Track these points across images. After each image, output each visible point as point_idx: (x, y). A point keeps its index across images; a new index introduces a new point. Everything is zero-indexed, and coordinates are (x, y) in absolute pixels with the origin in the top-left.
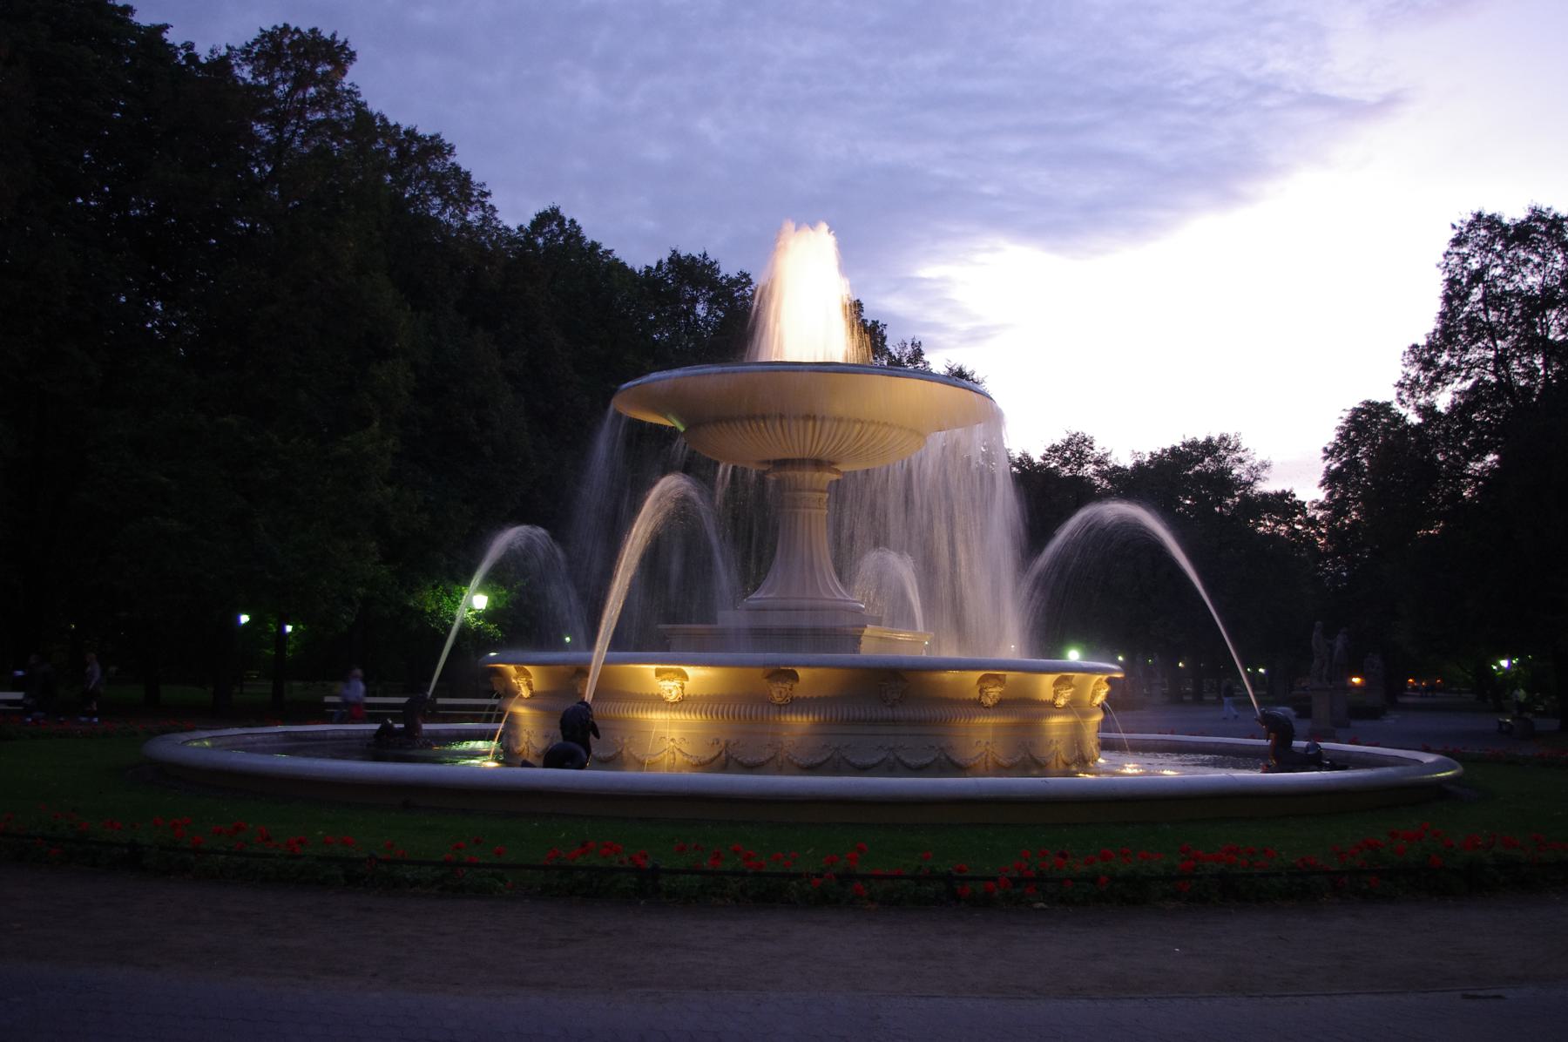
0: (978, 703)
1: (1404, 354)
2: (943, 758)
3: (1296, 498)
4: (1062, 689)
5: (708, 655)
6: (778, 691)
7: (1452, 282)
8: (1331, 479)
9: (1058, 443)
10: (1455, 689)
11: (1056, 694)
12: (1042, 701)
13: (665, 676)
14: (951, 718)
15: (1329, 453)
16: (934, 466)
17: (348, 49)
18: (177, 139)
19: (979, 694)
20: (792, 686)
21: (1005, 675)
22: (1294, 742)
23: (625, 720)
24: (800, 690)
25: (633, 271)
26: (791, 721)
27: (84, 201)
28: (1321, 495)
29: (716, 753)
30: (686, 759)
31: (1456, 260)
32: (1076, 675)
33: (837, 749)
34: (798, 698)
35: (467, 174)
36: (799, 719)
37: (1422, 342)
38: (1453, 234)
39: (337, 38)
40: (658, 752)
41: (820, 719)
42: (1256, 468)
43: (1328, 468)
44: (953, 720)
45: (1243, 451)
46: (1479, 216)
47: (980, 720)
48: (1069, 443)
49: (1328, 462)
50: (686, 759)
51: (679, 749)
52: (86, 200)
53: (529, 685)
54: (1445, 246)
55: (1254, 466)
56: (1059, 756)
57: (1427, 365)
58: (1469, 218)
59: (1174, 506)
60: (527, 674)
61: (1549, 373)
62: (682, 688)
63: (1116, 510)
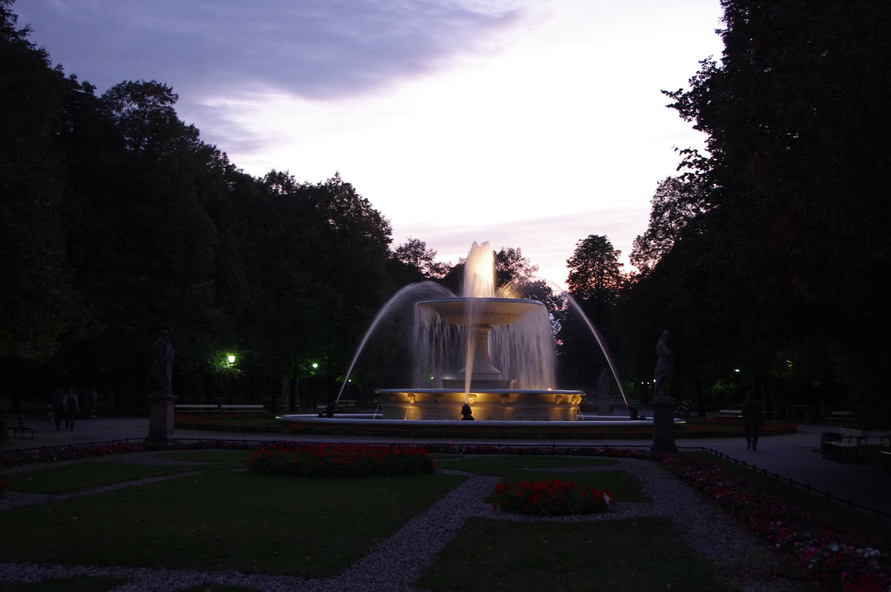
0: (555, 403)
1: (634, 242)
3: (546, 285)
5: (480, 390)
6: (503, 400)
7: (656, 207)
8: (573, 279)
9: (403, 246)
10: (116, 443)
11: (556, 400)
15: (571, 264)
24: (510, 401)
25: (253, 179)
28: (566, 287)
31: (659, 199)
32: (563, 395)
37: (642, 235)
38: (657, 186)
39: (167, 86)
42: (530, 270)
43: (571, 272)
45: (522, 260)
46: (669, 179)
47: (556, 408)
48: (411, 245)
49: (570, 269)
54: (654, 193)
55: (529, 269)
57: (645, 246)
58: (665, 179)
59: (363, 236)
60: (414, 396)
63: (430, 283)
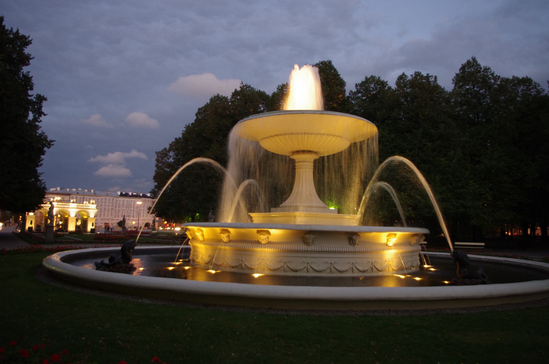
12: (383, 243)
13: (261, 233)
14: (379, 250)
17: (391, 89)
18: (22, 97)
19: (386, 240)
22: (457, 262)
23: (253, 251)
24: (271, 239)
26: (265, 250)
34: (231, 240)
36: (268, 250)
41: (278, 250)
44: (379, 252)
53: (203, 235)
56: (390, 267)
61: (460, 121)
62: (268, 238)
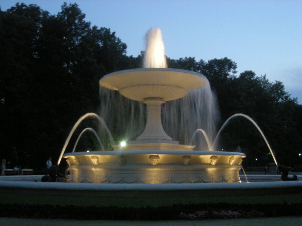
2: (200, 180)
4: (213, 160)
16: (200, 112)
20: (158, 160)
21: (217, 156)
27: (73, 63)
29: (168, 180)
30: (160, 182)
33: (123, 178)
35: (245, 72)
40: (205, 180)
50: (160, 182)
51: (156, 179)
52: (74, 63)
